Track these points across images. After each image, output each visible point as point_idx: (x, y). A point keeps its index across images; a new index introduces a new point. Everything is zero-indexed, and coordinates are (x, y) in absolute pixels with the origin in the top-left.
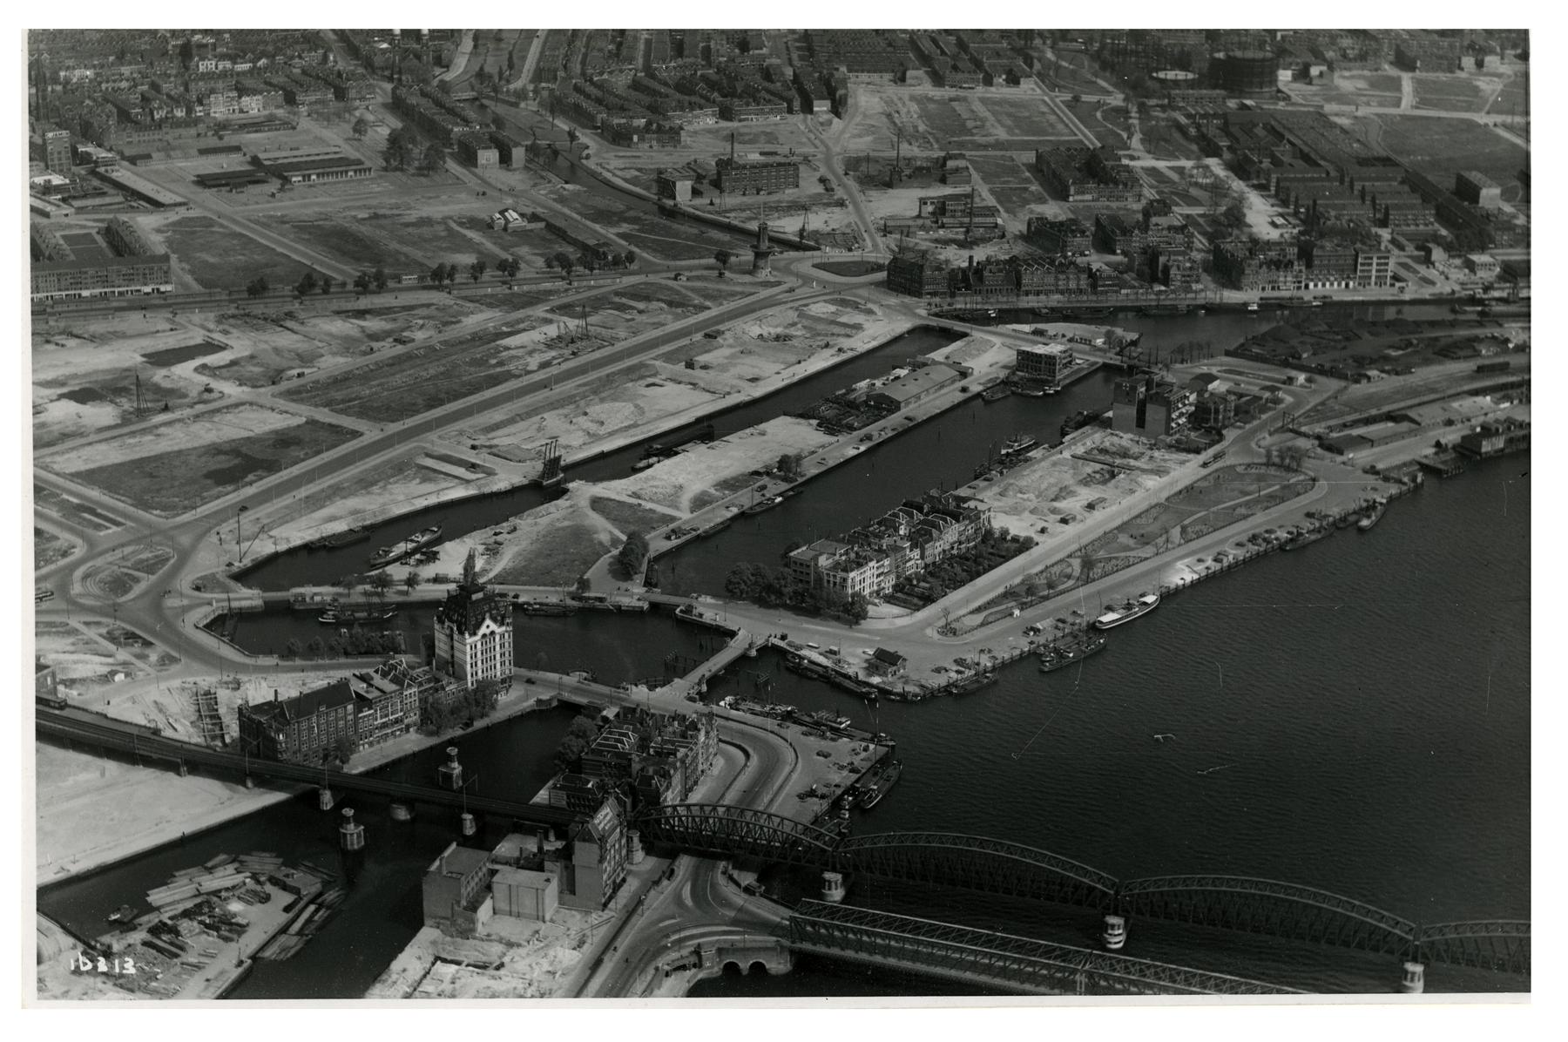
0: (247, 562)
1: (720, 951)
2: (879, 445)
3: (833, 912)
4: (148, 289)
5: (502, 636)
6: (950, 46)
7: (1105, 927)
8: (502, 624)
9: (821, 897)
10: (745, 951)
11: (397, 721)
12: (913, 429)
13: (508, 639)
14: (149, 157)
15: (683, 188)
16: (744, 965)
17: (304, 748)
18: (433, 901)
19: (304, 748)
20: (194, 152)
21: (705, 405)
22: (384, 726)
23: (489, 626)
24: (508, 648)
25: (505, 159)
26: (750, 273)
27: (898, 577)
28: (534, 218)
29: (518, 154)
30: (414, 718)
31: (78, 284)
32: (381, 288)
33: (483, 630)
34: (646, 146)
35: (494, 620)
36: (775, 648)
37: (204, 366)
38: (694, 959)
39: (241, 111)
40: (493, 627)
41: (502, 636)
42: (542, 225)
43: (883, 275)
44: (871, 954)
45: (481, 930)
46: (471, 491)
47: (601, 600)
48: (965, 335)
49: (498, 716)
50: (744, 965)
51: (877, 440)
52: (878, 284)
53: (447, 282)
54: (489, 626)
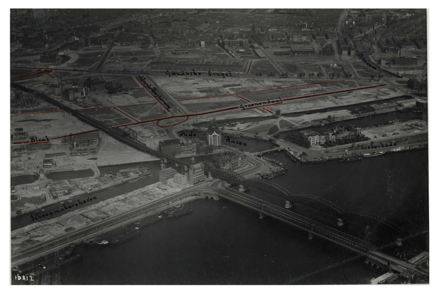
0: (198, 122)
1: (205, 193)
2: (362, 118)
3: (240, 194)
4: (237, 73)
5: (218, 136)
6: (12, 22)
7: (285, 203)
8: (218, 134)
9: (238, 190)
10: (209, 194)
11: (191, 150)
12: (375, 115)
13: (220, 137)
14: (268, 48)
15: (383, 62)
16: (210, 197)
17: (168, 151)
18: (161, 177)
19: (168, 151)
20: (279, 47)
21: (334, 105)
22: (187, 150)
23: (215, 134)
24: (220, 139)
25: (349, 54)
26: (378, 81)
27: (326, 141)
28: (339, 66)
29: (353, 52)
30: (195, 150)
31: (222, 70)
32: (286, 77)
33: (213, 134)
34: (389, 53)
35: (217, 133)
36: (286, 150)
37: (233, 88)
38: (198, 194)
39: (301, 40)
40: (216, 134)
41: (218, 136)
42: (341, 68)
43: (406, 84)
44: (320, 234)
45: (168, 184)
46: (258, 116)
47: (259, 137)
48: (414, 98)
49: (213, 154)
50: (210, 197)
51: (361, 116)
52: (405, 86)
53: (302, 77)
54: (215, 134)
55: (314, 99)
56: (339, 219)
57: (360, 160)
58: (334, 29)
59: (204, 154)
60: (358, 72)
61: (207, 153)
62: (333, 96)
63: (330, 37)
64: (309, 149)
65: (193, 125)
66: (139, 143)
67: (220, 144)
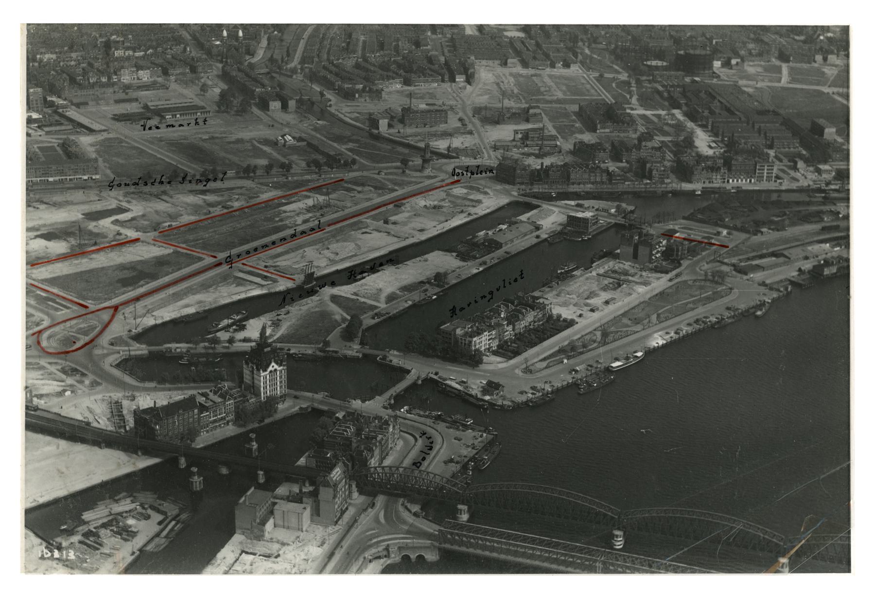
0: (140, 329)
3: (462, 527)
4: (86, 177)
5: (281, 371)
7: (613, 536)
8: (280, 365)
9: (455, 518)
11: (222, 419)
14: (87, 104)
15: (383, 124)
16: (413, 556)
22: (215, 421)
23: (273, 366)
25: (285, 107)
26: (420, 171)
28: (300, 139)
29: (292, 104)
30: (231, 417)
33: (270, 368)
34: (363, 100)
35: (277, 364)
37: (117, 221)
39: (138, 79)
40: (276, 367)
41: (281, 371)
42: (305, 143)
51: (489, 264)
53: (252, 174)
54: (273, 366)
55: (341, 230)
56: (460, 507)
57: (612, 382)
58: (185, 49)
59: (257, 425)
60: (347, 149)
61: (262, 421)
62: (374, 218)
63: (200, 69)
64: (483, 367)
65: (138, 338)
66: (58, 419)
67: (285, 390)
